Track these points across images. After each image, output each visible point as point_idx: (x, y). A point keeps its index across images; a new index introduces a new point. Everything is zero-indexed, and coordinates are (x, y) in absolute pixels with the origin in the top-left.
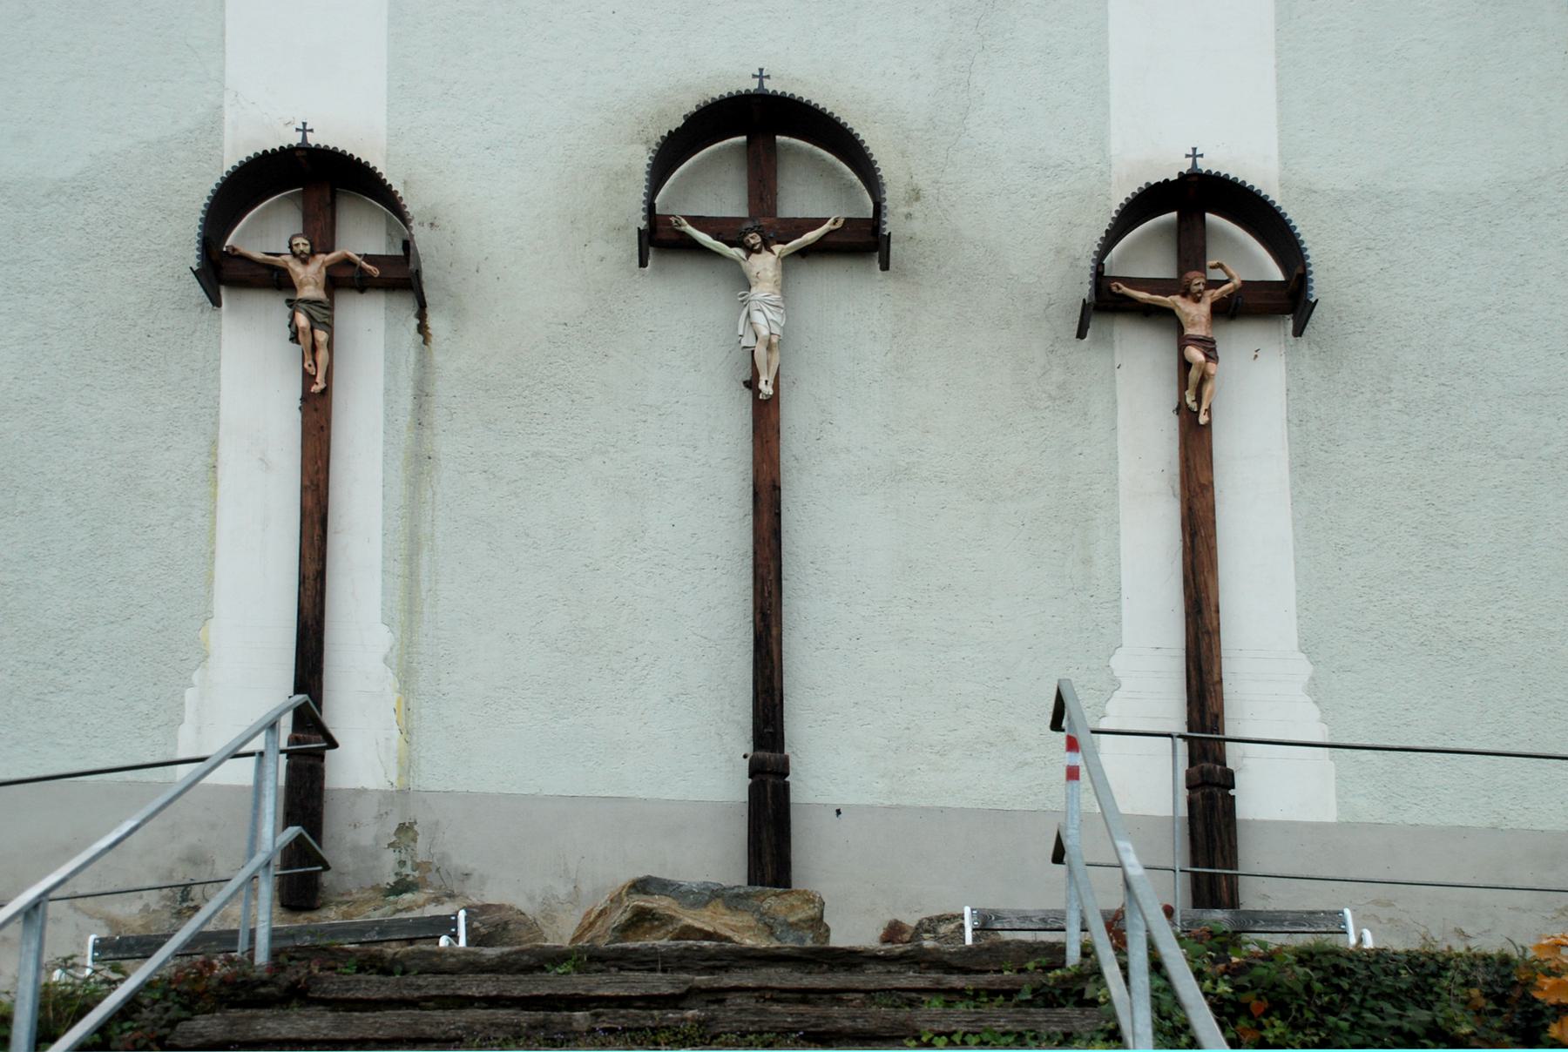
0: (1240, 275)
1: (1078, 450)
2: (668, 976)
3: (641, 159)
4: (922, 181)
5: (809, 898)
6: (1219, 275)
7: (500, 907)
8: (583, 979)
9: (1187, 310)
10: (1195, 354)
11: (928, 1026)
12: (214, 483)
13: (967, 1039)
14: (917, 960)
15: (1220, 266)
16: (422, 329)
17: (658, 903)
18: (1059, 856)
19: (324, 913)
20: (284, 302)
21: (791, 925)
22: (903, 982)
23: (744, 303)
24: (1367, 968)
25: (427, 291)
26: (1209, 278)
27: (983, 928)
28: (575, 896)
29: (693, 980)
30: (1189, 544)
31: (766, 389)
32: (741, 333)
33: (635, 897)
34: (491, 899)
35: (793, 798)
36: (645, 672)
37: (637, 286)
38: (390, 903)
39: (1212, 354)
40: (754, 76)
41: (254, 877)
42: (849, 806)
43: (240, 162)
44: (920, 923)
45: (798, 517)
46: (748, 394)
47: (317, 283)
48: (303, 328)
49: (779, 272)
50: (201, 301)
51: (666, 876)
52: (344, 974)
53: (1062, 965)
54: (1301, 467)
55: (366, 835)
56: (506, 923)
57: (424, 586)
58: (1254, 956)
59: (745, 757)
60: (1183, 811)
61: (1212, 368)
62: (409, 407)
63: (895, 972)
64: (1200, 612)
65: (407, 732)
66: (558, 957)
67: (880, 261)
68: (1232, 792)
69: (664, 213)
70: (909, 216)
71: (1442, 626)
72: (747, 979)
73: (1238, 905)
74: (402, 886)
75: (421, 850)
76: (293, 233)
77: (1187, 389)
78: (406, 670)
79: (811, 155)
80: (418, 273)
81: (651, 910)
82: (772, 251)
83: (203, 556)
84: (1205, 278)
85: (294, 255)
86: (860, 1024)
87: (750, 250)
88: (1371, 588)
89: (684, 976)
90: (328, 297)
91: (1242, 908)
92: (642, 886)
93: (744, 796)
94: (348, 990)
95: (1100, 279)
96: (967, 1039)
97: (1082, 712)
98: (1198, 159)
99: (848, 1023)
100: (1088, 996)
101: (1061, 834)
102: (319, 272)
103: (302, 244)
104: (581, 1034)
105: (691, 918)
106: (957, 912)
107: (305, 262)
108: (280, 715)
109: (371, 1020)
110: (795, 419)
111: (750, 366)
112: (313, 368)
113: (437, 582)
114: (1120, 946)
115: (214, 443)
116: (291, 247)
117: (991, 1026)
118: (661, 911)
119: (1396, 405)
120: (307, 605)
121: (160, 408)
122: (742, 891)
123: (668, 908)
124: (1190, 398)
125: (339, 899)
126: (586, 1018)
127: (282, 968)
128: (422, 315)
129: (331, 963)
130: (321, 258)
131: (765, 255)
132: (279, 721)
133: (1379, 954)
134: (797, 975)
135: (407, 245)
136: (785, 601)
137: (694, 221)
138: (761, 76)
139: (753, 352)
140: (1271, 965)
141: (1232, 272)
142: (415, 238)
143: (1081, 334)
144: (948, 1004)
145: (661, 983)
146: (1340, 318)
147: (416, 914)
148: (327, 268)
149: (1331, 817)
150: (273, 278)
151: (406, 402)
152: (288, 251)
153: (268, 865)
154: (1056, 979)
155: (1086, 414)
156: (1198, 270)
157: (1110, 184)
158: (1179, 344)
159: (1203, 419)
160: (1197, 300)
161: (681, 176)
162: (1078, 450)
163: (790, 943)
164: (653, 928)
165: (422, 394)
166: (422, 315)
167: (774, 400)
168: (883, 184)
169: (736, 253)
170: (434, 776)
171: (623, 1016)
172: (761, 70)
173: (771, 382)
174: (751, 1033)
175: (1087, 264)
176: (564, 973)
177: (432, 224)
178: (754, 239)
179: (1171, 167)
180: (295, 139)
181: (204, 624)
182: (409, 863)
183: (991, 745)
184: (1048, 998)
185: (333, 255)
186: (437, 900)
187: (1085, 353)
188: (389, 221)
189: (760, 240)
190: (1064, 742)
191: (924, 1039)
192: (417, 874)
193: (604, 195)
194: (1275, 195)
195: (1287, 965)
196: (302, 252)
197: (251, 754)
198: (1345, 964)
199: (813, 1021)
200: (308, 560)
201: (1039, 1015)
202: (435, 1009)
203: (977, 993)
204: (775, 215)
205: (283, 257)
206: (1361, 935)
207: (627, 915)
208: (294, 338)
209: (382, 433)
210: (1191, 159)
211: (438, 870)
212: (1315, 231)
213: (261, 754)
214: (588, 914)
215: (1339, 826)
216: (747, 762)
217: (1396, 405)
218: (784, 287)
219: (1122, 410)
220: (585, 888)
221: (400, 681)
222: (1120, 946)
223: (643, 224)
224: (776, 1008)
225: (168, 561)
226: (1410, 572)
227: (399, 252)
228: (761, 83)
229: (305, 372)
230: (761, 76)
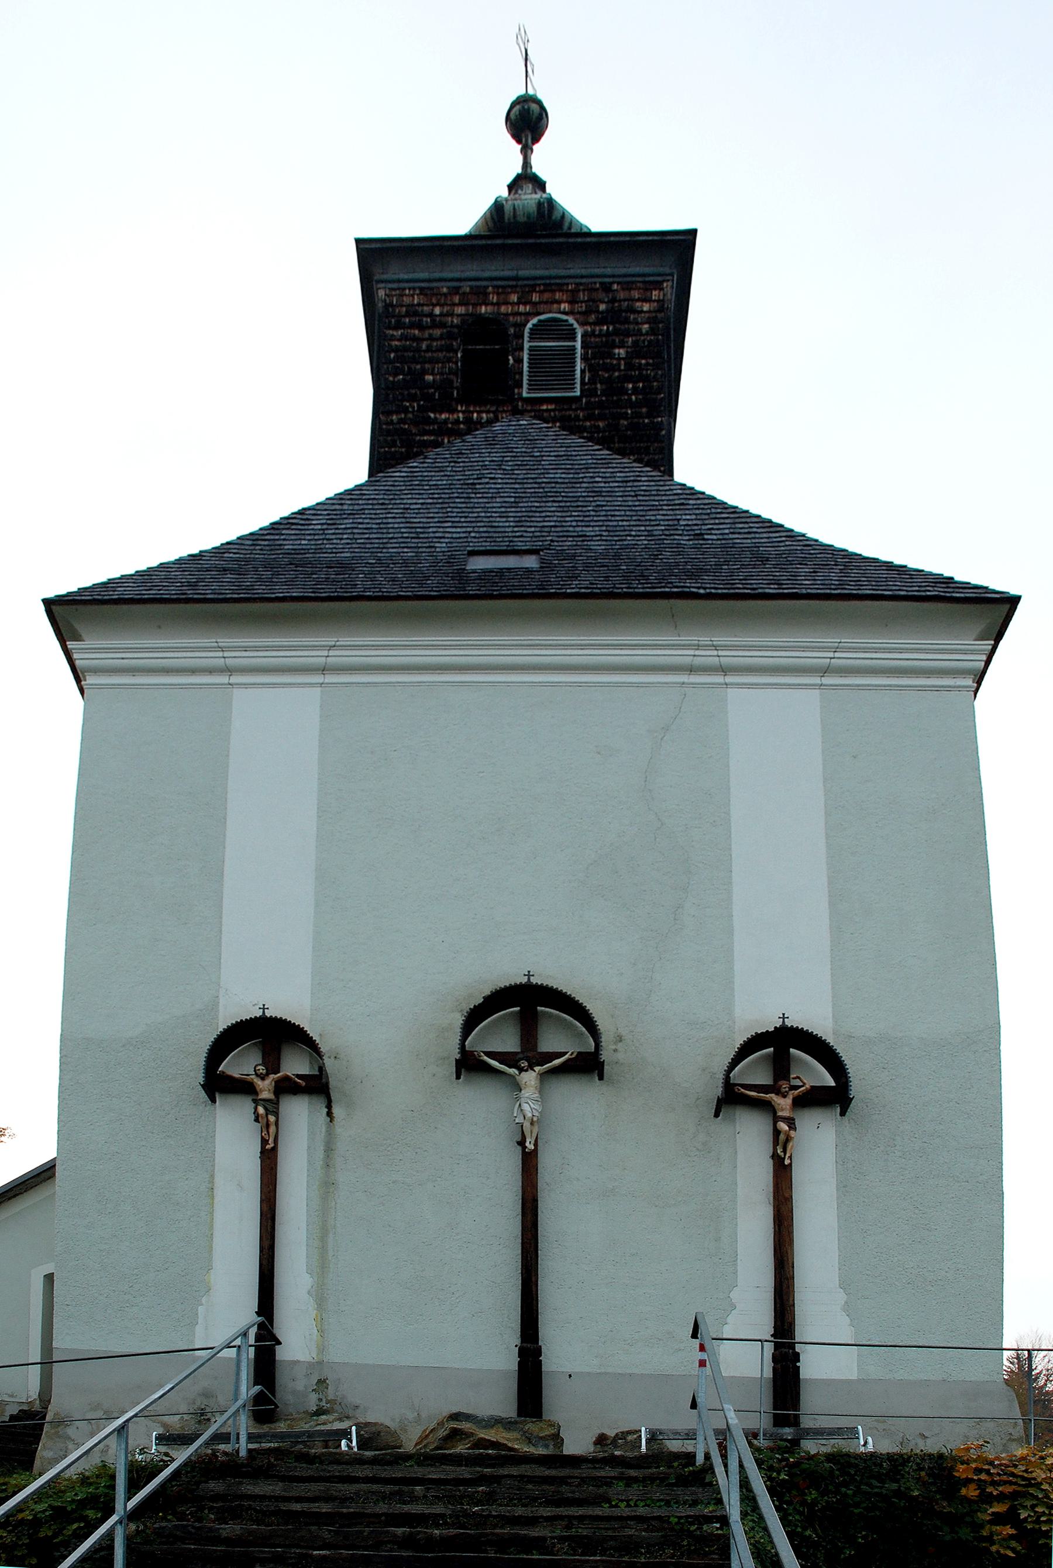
0: (810, 1082)
1: (714, 1178)
2: (468, 1469)
3: (458, 1020)
4: (623, 1031)
5: (551, 1425)
6: (798, 1083)
7: (375, 1424)
8: (420, 1469)
9: (779, 1102)
10: (783, 1126)
11: (615, 1496)
12: (213, 1198)
13: (638, 1503)
14: (612, 1461)
15: (798, 1078)
16: (330, 1114)
17: (465, 1426)
18: (694, 1405)
19: (277, 1424)
20: (250, 1101)
21: (541, 1438)
22: (603, 1473)
23: (518, 1099)
24: (865, 1463)
25: (332, 1094)
26: (792, 1084)
27: (653, 1437)
28: (418, 1419)
29: (482, 1471)
30: (777, 1229)
31: (530, 1146)
32: (515, 1115)
33: (451, 1422)
34: (371, 1419)
35: (544, 1369)
36: (458, 1301)
37: (454, 1090)
38: (314, 1420)
39: (792, 1126)
40: (525, 975)
41: (238, 1411)
42: (576, 1373)
43: (228, 1026)
44: (617, 1435)
45: (548, 1216)
46: (519, 1148)
47: (269, 1090)
48: (262, 1114)
49: (538, 1082)
50: (204, 1100)
51: (470, 1412)
52: (288, 1463)
53: (693, 1464)
54: (843, 1187)
55: (300, 1385)
56: (379, 1432)
57: (331, 1253)
58: (802, 1458)
59: (516, 1346)
60: (768, 1373)
61: (792, 1133)
62: (322, 1157)
63: (598, 1468)
64: (783, 1267)
65: (321, 1331)
66: (407, 1457)
67: (598, 1076)
68: (798, 1364)
69: (471, 1050)
70: (615, 1050)
71: (921, 1273)
72: (514, 1471)
73: (799, 1423)
74: (320, 1412)
75: (331, 1393)
76: (256, 1063)
77: (778, 1145)
78: (320, 1296)
79: (558, 1017)
80: (327, 1084)
81: (460, 1429)
82: (535, 1071)
83: (207, 1236)
84: (789, 1085)
85: (257, 1075)
86: (577, 1495)
87: (521, 1070)
88: (881, 1253)
89: (478, 1469)
90: (276, 1097)
91: (802, 1426)
92: (455, 1417)
93: (515, 1367)
94: (290, 1471)
95: (728, 1085)
96: (638, 1503)
97: (709, 1329)
98: (786, 1019)
99: (570, 1495)
100: (707, 1481)
101: (696, 1395)
102: (271, 1084)
103: (262, 1069)
104: (419, 1498)
105: (483, 1434)
106: (637, 1428)
107: (263, 1079)
108: (249, 1328)
109: (303, 1487)
110: (546, 1163)
111: (520, 1133)
112: (267, 1136)
113: (338, 1251)
114: (724, 1457)
115: (212, 1176)
116: (255, 1071)
117: (651, 1497)
118: (466, 1430)
119: (898, 1154)
120: (264, 1263)
121: (183, 1157)
122: (513, 1420)
123: (470, 1429)
124: (779, 1151)
125: (286, 1418)
126: (422, 1491)
127: (254, 1459)
128: (329, 1107)
129: (281, 1457)
130: (272, 1076)
131: (530, 1072)
132: (248, 1331)
133: (873, 1455)
134: (543, 1469)
135: (321, 1069)
136: (540, 1262)
137: (488, 1054)
138: (529, 975)
139: (522, 1126)
140: (811, 1462)
141: (805, 1081)
142: (326, 1065)
143: (717, 1115)
144: (628, 1485)
145: (464, 1472)
146: (867, 1106)
147: (328, 1427)
148: (275, 1082)
149: (854, 1375)
150: (243, 1088)
151: (320, 1154)
152: (254, 1073)
153: (245, 1406)
154: (690, 1471)
155: (718, 1159)
156: (787, 1081)
157: (734, 1033)
158: (773, 1120)
159: (787, 1162)
160: (784, 1096)
161: (481, 1029)
162: (714, 1178)
163: (541, 1451)
164: (462, 1439)
165: (329, 1149)
166: (329, 1107)
167: (535, 1151)
168: (600, 1033)
169: (513, 1071)
170: (336, 1354)
171: (442, 1490)
172: (529, 972)
173: (533, 1142)
174: (515, 1500)
175: (721, 1076)
176: (410, 1466)
177: (335, 1057)
178: (524, 1064)
179: (770, 1023)
180: (259, 1013)
181: (208, 1272)
182: (324, 1400)
183: (660, 1340)
184: (684, 1481)
185: (279, 1075)
186: (340, 1420)
187: (719, 1126)
188: (311, 1055)
189: (527, 1064)
190: (698, 1346)
191: (613, 1503)
192: (328, 1405)
193: (436, 1040)
194: (831, 1040)
195: (820, 1463)
196: (261, 1074)
197: (235, 1347)
198: (853, 1461)
199: (551, 1493)
200: (264, 1239)
201: (679, 1491)
202: (337, 1483)
203: (644, 1479)
204: (536, 1051)
205: (251, 1076)
206: (867, 1443)
207: (447, 1432)
208: (257, 1120)
209: (306, 1171)
210: (781, 1019)
211: (340, 1404)
212: (854, 1059)
213: (239, 1347)
214: (425, 1431)
215: (859, 1380)
216: (517, 1348)
217: (898, 1154)
218: (541, 1090)
219: (740, 1157)
220: (424, 1415)
221: (317, 1304)
222: (724, 1457)
223: (458, 1056)
224: (530, 1486)
225: (187, 1239)
226: (903, 1244)
227: (317, 1073)
228: (529, 979)
229: (262, 1137)
230: (529, 975)
